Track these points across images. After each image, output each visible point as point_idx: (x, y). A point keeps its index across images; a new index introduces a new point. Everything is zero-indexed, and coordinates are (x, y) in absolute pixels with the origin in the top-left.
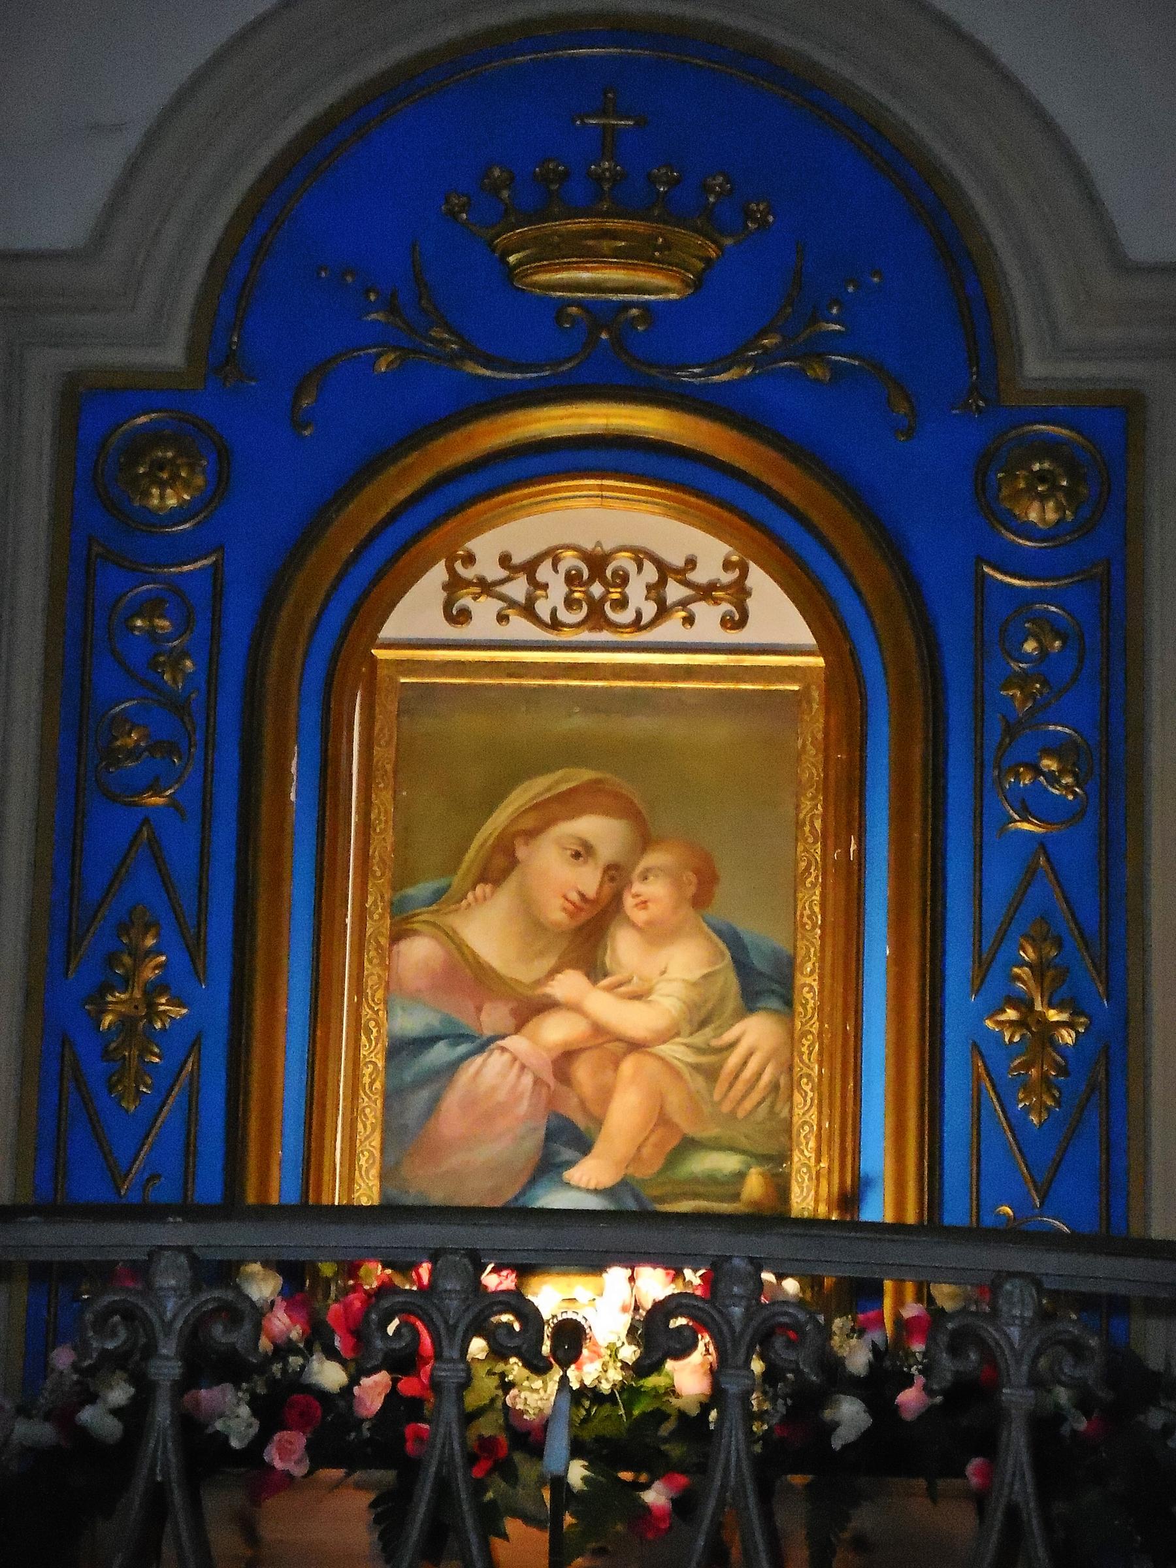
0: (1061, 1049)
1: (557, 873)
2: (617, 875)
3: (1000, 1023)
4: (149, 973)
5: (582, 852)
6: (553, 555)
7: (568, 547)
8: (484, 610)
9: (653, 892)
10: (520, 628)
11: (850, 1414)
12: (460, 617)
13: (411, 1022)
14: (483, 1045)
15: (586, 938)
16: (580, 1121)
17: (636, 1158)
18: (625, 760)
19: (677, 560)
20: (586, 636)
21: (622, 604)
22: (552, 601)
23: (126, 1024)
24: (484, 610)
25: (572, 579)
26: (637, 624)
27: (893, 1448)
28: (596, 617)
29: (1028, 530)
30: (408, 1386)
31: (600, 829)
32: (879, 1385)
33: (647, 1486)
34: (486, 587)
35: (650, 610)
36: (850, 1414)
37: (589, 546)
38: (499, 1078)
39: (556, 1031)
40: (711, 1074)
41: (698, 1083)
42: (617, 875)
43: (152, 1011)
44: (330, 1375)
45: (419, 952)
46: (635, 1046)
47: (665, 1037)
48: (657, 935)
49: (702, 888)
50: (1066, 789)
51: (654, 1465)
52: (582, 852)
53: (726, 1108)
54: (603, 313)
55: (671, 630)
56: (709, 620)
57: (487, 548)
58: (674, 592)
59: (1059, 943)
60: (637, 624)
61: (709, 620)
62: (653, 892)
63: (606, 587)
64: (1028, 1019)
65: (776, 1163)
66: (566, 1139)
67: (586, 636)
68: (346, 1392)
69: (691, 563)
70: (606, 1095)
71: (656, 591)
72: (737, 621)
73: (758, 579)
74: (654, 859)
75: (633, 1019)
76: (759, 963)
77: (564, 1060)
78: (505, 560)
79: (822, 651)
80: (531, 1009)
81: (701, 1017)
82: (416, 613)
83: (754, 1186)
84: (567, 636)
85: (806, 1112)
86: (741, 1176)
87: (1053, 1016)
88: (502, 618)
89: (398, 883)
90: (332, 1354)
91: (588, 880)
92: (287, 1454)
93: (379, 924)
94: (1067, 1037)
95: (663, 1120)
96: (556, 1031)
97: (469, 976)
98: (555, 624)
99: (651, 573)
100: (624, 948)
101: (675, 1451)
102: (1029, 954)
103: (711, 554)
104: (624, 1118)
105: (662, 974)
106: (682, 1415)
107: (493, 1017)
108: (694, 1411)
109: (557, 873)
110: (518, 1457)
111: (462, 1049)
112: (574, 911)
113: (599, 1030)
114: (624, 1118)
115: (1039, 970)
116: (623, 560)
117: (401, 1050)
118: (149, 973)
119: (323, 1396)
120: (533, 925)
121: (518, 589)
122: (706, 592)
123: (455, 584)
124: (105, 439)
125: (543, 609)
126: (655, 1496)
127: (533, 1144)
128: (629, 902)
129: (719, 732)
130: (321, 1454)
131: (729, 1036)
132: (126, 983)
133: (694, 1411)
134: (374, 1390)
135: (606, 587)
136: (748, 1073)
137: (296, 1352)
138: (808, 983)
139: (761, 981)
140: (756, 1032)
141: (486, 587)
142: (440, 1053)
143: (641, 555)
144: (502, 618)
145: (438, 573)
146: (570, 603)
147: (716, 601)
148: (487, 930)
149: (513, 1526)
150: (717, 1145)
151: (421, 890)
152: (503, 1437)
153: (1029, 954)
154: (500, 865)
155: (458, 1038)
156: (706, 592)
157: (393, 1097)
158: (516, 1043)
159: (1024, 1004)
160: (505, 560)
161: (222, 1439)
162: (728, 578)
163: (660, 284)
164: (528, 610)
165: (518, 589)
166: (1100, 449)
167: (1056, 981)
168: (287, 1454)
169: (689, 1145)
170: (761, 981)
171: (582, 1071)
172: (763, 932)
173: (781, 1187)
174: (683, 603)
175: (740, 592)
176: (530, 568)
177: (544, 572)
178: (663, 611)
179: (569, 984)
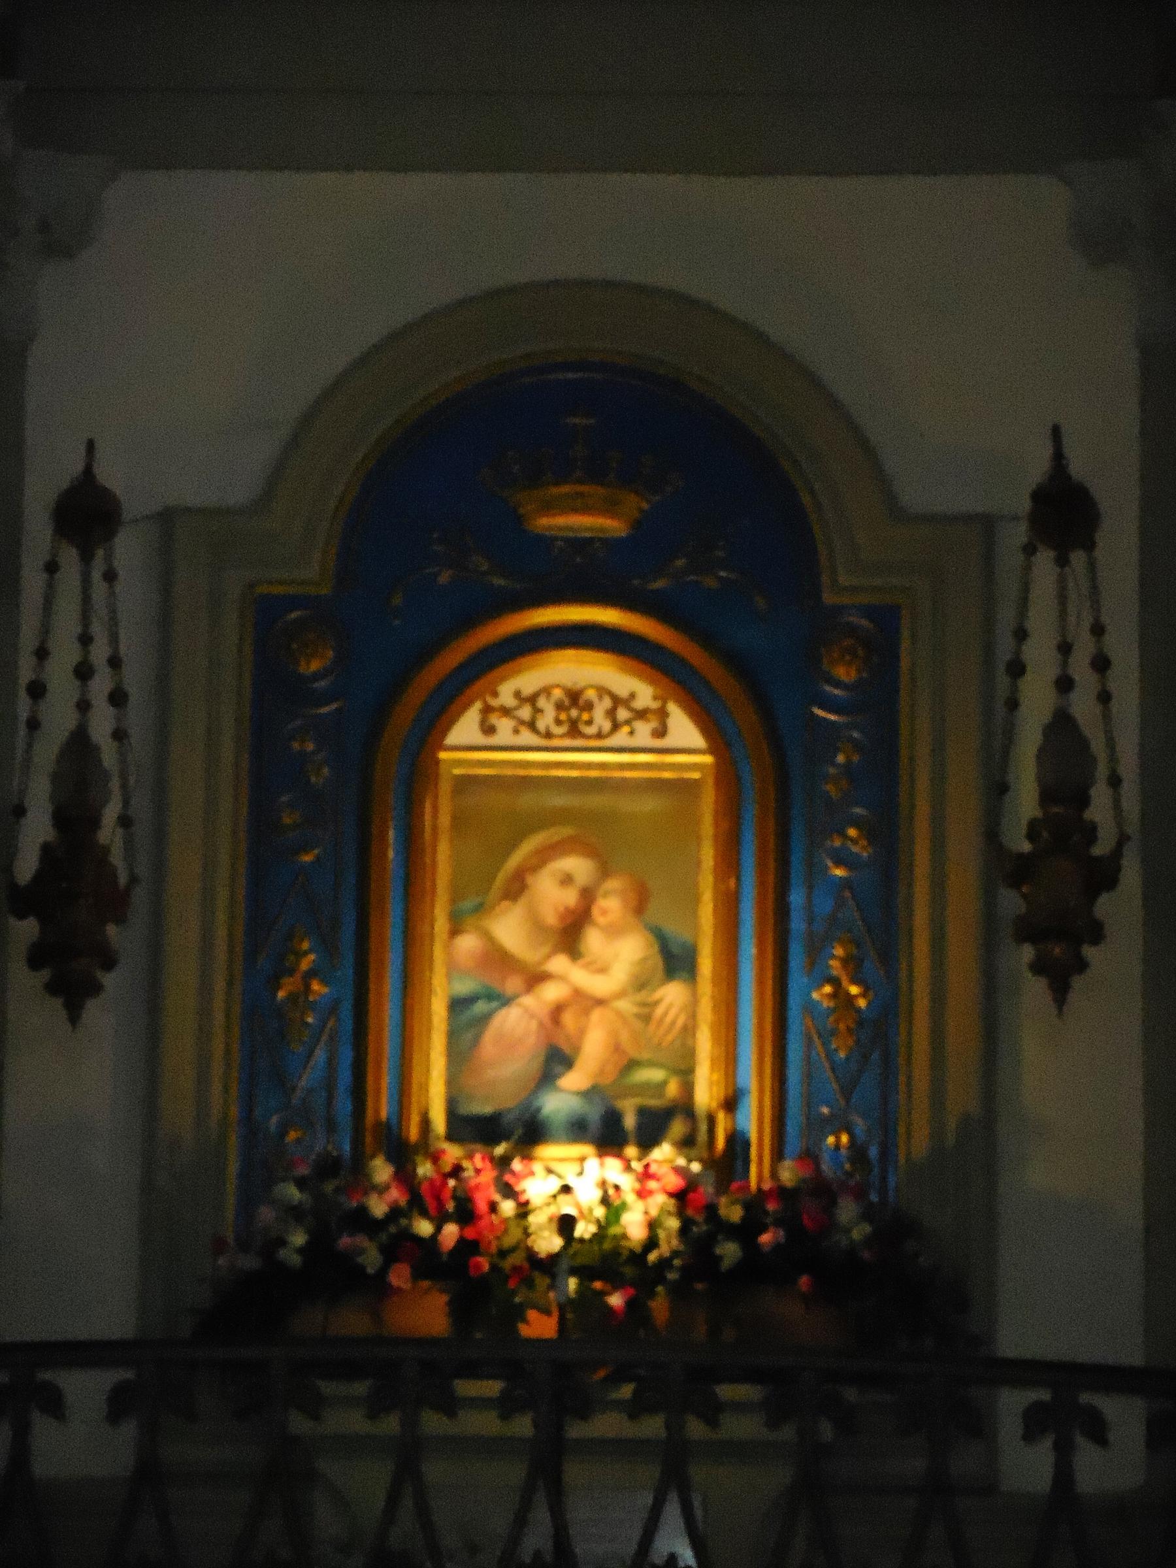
0: (858, 1010)
1: (551, 893)
2: (588, 896)
3: (822, 995)
4: (305, 964)
5: (567, 880)
6: (546, 691)
7: (558, 686)
8: (504, 725)
9: (611, 905)
10: (527, 737)
11: (729, 1251)
12: (489, 730)
13: (464, 987)
14: (506, 1001)
15: (570, 934)
16: (566, 1049)
17: (602, 1072)
18: (592, 819)
19: (623, 693)
20: (567, 742)
21: (589, 722)
22: (546, 721)
23: (293, 998)
24: (504, 725)
25: (559, 707)
26: (599, 736)
27: (755, 1266)
28: (574, 730)
29: (838, 684)
30: (470, 1233)
31: (577, 866)
32: (746, 1232)
33: (610, 1294)
34: (506, 712)
35: (607, 726)
36: (729, 1251)
37: (569, 684)
38: (517, 1023)
39: (552, 992)
40: (646, 1018)
41: (638, 1025)
42: (588, 896)
43: (307, 989)
44: (424, 1228)
45: (468, 943)
46: (600, 1002)
47: (621, 994)
48: (614, 932)
49: (640, 903)
50: (861, 850)
51: (616, 1282)
52: (567, 880)
53: (656, 1040)
54: (580, 545)
55: (621, 738)
56: (643, 732)
57: (506, 694)
58: (623, 714)
59: (858, 946)
60: (599, 736)
61: (643, 732)
62: (611, 905)
63: (581, 720)
64: (839, 993)
65: (686, 1074)
66: (556, 1059)
67: (567, 742)
68: (434, 1237)
69: (633, 696)
70: (582, 1032)
71: (611, 713)
72: (661, 732)
73: (673, 709)
74: (613, 884)
75: (598, 985)
76: (675, 950)
77: (557, 1011)
78: (517, 694)
79: (711, 750)
80: (536, 978)
81: (640, 983)
82: (465, 729)
83: (673, 1089)
84: (556, 742)
85: (705, 1044)
86: (663, 1084)
87: (854, 990)
88: (516, 731)
89: (453, 901)
90: (425, 1214)
91: (570, 898)
92: (399, 1277)
93: (441, 924)
94: (862, 1003)
95: (617, 1048)
96: (552, 992)
97: (497, 958)
98: (548, 735)
99: (607, 703)
100: (593, 940)
101: (628, 1271)
102: (839, 951)
103: (645, 694)
104: (594, 1048)
105: (617, 955)
106: (631, 1251)
107: (513, 984)
108: (638, 1250)
109: (551, 893)
110: (536, 1274)
111: (494, 1004)
112: (562, 918)
113: (578, 994)
114: (594, 1048)
115: (845, 961)
116: (591, 694)
117: (457, 1005)
118: (305, 964)
119: (418, 1240)
120: (537, 925)
121: (525, 713)
122: (642, 714)
123: (487, 710)
124: (273, 627)
125: (541, 725)
126: (616, 1300)
127: (536, 1066)
128: (595, 911)
129: (649, 804)
130: (419, 1274)
131: (658, 994)
132: (291, 972)
133: (638, 1250)
134: (451, 1231)
135: (581, 720)
136: (669, 1019)
137: (405, 1216)
138: (706, 964)
139: (676, 961)
140: (673, 994)
141: (506, 712)
142: (480, 1007)
143: (603, 691)
144: (516, 731)
145: (478, 705)
146: (558, 722)
147: (648, 720)
148: (509, 929)
149: (532, 1315)
150: (651, 1064)
151: (468, 904)
152: (526, 1265)
153: (839, 951)
154: (517, 888)
155: (490, 996)
156: (642, 714)
157: (453, 1036)
158: (528, 1000)
159: (835, 982)
160: (517, 694)
161: (362, 1268)
162: (655, 705)
163: (611, 525)
164: (532, 726)
165: (525, 713)
166: (880, 642)
167: (855, 967)
168: (399, 1277)
169: (632, 1064)
170: (676, 961)
171: (568, 1019)
172: (676, 929)
173: (688, 1088)
174: (628, 722)
175: (663, 714)
176: (532, 699)
177: (542, 702)
178: (616, 727)
179: (559, 963)
